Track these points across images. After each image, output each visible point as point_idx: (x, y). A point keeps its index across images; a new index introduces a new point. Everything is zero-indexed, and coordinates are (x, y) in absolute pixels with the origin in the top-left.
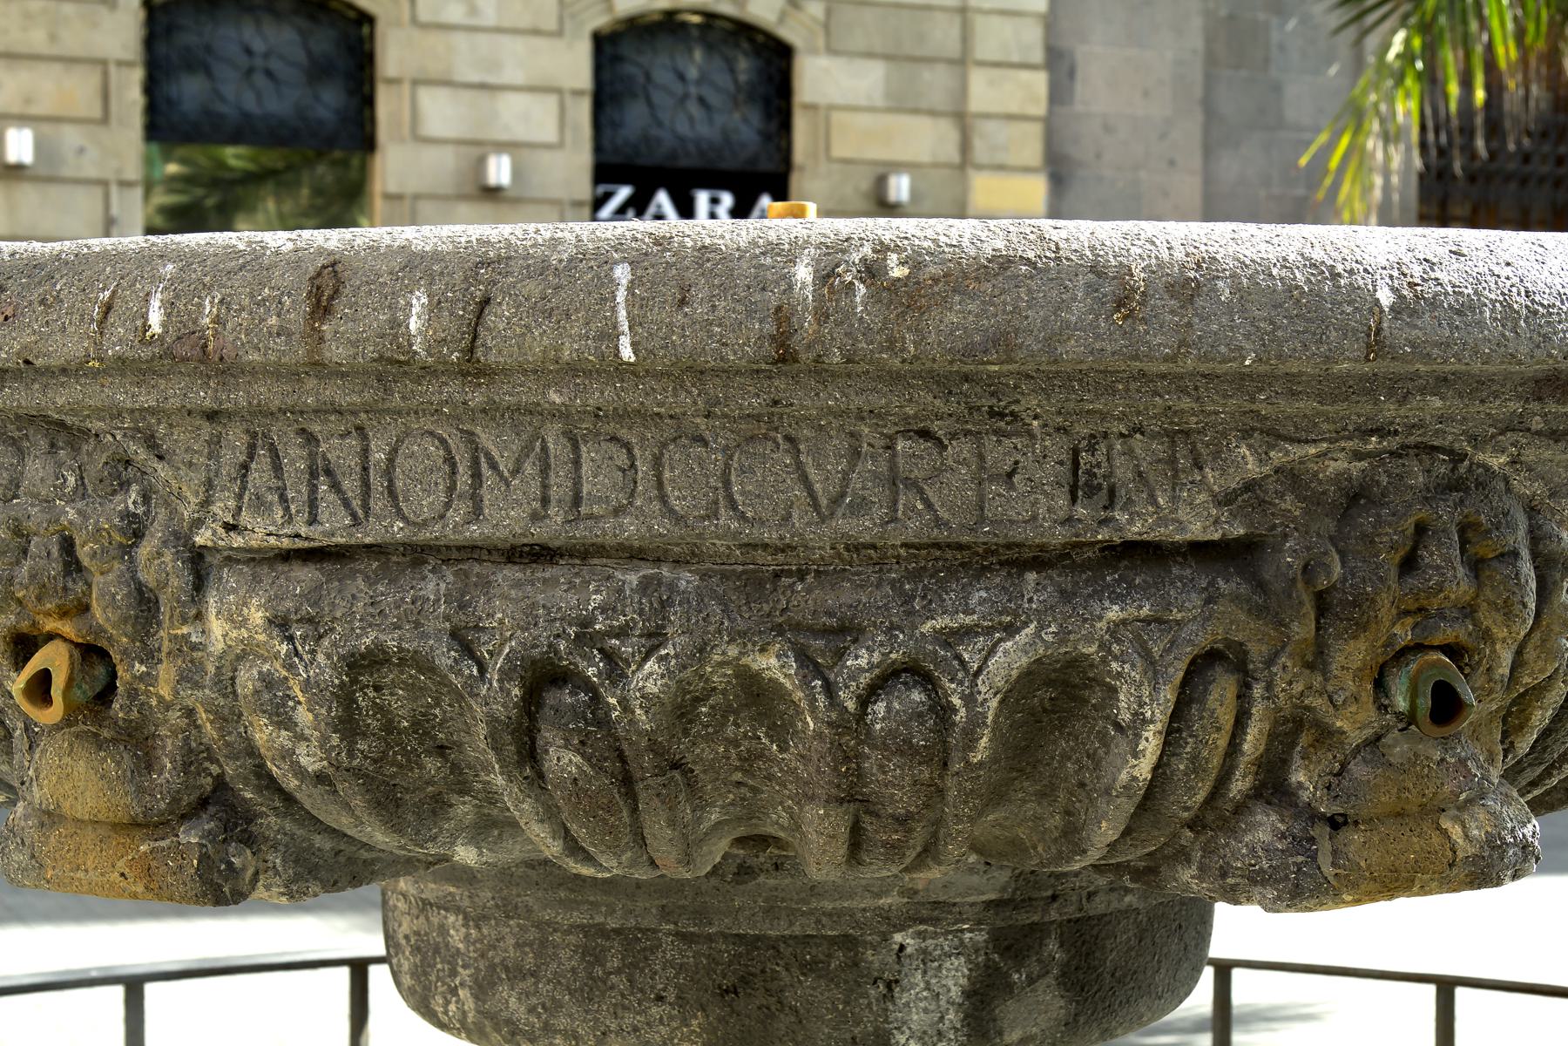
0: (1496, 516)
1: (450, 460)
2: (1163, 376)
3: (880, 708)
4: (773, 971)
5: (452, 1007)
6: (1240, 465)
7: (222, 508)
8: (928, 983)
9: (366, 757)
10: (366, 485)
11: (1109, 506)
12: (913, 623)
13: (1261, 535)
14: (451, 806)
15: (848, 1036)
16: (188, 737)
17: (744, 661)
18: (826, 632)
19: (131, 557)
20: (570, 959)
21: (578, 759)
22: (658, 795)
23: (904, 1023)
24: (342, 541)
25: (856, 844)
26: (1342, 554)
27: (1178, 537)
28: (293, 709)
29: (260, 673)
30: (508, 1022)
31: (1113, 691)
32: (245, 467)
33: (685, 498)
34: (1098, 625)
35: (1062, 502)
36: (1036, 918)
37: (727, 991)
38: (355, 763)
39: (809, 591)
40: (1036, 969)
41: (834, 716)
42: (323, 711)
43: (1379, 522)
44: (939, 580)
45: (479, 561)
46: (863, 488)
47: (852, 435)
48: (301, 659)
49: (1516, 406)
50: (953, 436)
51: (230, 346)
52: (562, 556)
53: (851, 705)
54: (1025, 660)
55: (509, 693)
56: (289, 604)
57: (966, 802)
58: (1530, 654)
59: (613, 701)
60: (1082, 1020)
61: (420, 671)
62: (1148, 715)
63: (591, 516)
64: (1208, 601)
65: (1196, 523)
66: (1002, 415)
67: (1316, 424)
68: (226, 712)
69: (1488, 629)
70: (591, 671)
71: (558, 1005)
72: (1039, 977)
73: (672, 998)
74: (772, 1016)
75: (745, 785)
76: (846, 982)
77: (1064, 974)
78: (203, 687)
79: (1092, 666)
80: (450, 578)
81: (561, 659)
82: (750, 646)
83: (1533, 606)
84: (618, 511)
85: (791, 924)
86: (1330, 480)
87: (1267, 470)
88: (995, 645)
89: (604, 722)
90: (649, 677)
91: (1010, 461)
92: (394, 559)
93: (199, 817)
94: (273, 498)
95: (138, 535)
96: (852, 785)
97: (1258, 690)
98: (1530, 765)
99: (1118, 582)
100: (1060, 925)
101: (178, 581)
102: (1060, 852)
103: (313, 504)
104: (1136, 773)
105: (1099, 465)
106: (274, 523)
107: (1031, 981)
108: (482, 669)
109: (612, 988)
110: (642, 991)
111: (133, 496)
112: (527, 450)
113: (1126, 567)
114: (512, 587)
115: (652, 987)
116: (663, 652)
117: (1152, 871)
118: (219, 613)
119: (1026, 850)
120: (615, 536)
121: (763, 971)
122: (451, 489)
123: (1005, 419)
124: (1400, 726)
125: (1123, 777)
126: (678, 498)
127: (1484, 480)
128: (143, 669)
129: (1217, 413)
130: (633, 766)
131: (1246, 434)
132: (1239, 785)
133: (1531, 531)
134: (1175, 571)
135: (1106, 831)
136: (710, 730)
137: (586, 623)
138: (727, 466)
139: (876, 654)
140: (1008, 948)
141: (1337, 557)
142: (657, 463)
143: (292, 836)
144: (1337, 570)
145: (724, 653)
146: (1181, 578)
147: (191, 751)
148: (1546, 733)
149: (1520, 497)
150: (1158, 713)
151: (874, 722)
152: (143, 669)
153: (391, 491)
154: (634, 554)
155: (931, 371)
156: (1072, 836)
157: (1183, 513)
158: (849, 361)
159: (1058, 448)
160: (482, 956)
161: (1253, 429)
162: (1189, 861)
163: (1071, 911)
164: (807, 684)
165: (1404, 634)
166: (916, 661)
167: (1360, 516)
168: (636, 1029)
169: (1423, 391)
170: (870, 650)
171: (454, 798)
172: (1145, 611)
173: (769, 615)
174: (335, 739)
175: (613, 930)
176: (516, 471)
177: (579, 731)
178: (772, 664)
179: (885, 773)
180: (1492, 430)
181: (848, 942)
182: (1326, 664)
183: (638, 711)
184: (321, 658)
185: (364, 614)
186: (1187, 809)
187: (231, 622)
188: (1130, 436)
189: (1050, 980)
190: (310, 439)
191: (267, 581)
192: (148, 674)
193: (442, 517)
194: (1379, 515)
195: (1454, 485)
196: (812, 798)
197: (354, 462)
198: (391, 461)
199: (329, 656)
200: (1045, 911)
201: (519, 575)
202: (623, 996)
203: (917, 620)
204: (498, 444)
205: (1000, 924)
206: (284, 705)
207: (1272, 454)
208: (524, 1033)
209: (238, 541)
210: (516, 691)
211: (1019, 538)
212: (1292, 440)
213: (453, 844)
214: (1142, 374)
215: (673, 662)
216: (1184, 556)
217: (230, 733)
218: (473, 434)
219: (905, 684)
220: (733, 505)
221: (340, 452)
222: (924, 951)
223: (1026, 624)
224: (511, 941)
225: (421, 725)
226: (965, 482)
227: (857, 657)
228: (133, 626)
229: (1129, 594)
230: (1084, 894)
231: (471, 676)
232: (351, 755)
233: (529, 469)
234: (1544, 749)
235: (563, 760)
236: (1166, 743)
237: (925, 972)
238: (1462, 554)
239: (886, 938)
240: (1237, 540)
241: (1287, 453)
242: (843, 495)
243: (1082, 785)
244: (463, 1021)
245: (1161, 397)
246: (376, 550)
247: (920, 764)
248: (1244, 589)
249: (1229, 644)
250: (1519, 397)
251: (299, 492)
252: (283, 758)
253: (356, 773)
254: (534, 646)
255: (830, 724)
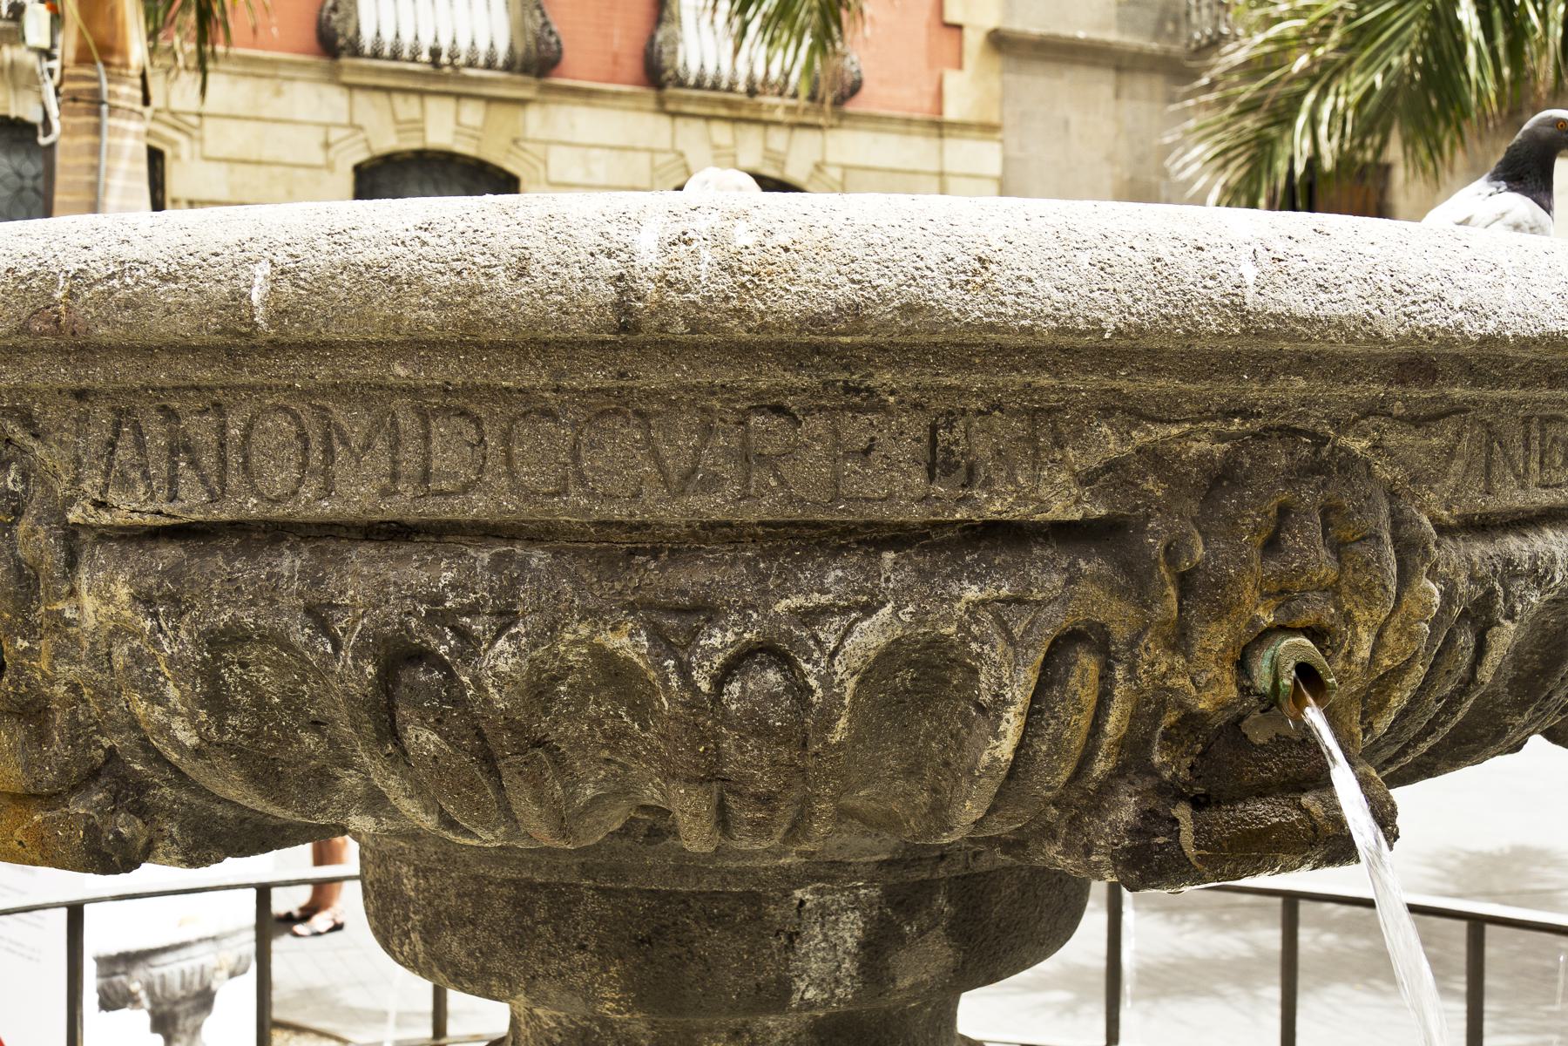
0: (1358, 500)
1: (302, 436)
2: (1021, 351)
3: (735, 688)
4: (685, 924)
5: (406, 948)
6: (1101, 442)
7: (91, 484)
8: (825, 935)
9: (238, 733)
10: (223, 461)
11: (969, 483)
12: (767, 602)
13: (1122, 516)
14: (337, 779)
15: (752, 983)
16: (75, 711)
17: (597, 640)
18: (679, 611)
19: (11, 534)
20: (503, 909)
21: (435, 737)
22: (520, 773)
23: (804, 971)
24: (200, 517)
25: (724, 820)
26: (1205, 535)
27: (1038, 517)
28: (164, 684)
29: (130, 649)
30: (452, 964)
31: (975, 672)
32: (112, 444)
33: (534, 474)
34: (957, 605)
35: (919, 479)
36: (925, 876)
37: (642, 941)
38: (226, 738)
39: (662, 569)
40: (926, 921)
41: (687, 695)
42: (188, 687)
43: (1242, 504)
44: (796, 559)
45: (337, 538)
46: (715, 464)
47: (703, 410)
48: (165, 636)
49: (1378, 390)
50: (808, 411)
51: (81, 320)
52: (418, 533)
53: (705, 686)
54: (883, 641)
55: (363, 672)
56: (152, 581)
57: (827, 783)
58: (1390, 637)
59: (465, 679)
60: (969, 966)
61: (281, 649)
62: (1009, 696)
63: (441, 493)
64: (1069, 581)
65: (1063, 504)
66: (857, 391)
67: (1178, 405)
68: (105, 687)
69: (1349, 612)
70: (443, 649)
71: (493, 951)
72: (929, 929)
73: (592, 946)
74: (684, 965)
75: (615, 762)
76: (750, 934)
77: (951, 926)
78: (80, 662)
79: (952, 646)
80: (306, 555)
81: (413, 637)
82: (601, 625)
83: (1393, 588)
84: (465, 489)
85: (699, 881)
86: (1192, 462)
87: (1128, 449)
88: (851, 625)
89: (459, 701)
90: (502, 657)
91: (865, 438)
92: (255, 535)
93: (88, 789)
94: (135, 475)
95: (18, 513)
96: (711, 765)
97: (1120, 673)
98: (1387, 744)
99: (977, 562)
100: (949, 881)
101: (53, 557)
102: (930, 828)
103: (173, 481)
104: (997, 754)
105: (957, 443)
106: (137, 500)
107: (921, 932)
108: (337, 646)
109: (540, 936)
110: (566, 940)
111: (13, 474)
112: (378, 425)
113: (986, 548)
114: (365, 564)
115: (575, 936)
116: (514, 631)
117: (1022, 844)
118: (89, 589)
119: (900, 823)
120: (464, 512)
121: (675, 924)
122: (303, 465)
123: (865, 400)
124: (1264, 706)
125: (985, 758)
126: (527, 474)
127: (1348, 462)
128: (26, 644)
129: (1078, 391)
130: (492, 744)
131: (1107, 412)
132: (1101, 766)
133: (1392, 515)
134: (1037, 551)
135: (970, 811)
136: (572, 709)
137: (437, 600)
138: (576, 441)
139: (729, 634)
140: (901, 903)
141: (1199, 538)
142: (506, 438)
143: (190, 805)
144: (1200, 552)
145: (575, 632)
146: (1042, 558)
147: (79, 724)
148: (1404, 714)
149: (1382, 482)
150: (1019, 694)
151: (729, 702)
152: (26, 644)
153: (245, 466)
154: (486, 532)
155: (781, 343)
156: (939, 813)
157: (1044, 491)
158: (693, 331)
159: (915, 426)
160: (430, 904)
161: (1114, 408)
162: (1054, 837)
163: (958, 869)
164: (660, 664)
165: (1267, 618)
166: (771, 641)
167: (1223, 497)
168: (561, 975)
169: (1287, 370)
170: (724, 630)
171: (339, 772)
172: (1005, 592)
173: (620, 593)
174: (203, 715)
175: (541, 884)
176: (367, 446)
177: (434, 709)
178: (626, 642)
179: (743, 753)
180: (1354, 414)
181: (753, 899)
182: (1189, 646)
183: (491, 690)
184: (183, 634)
185: (229, 591)
186: (1050, 789)
187: (99, 600)
188: (989, 413)
189: (939, 931)
190: (170, 414)
191: (133, 557)
192: (31, 649)
193: (295, 493)
194: (1242, 497)
195: (1315, 468)
196: (674, 776)
197: (211, 438)
198: (246, 437)
199: (190, 633)
200: (934, 870)
201: (373, 552)
202: (549, 944)
203: (771, 598)
204: (353, 421)
205: (891, 881)
206: (155, 681)
207: (1134, 433)
208: (464, 975)
209: (106, 518)
210: (370, 669)
211: (876, 517)
212: (1154, 420)
213: (345, 814)
214: (999, 348)
215: (524, 640)
216: (1046, 537)
217: (111, 708)
218: (326, 409)
219: (761, 663)
220: (581, 479)
221: (200, 429)
222: (822, 906)
223: (883, 604)
224: (453, 891)
225: (291, 700)
226: (819, 459)
227: (710, 637)
228: (14, 601)
229: (988, 574)
230: (970, 853)
231: (325, 653)
232: (221, 730)
233: (379, 445)
234: (1401, 729)
235: (423, 738)
236: (1027, 724)
237: (823, 925)
238: (1324, 537)
239: (787, 894)
240: (1100, 520)
241: (1149, 433)
242: (694, 471)
243: (947, 764)
244: (415, 961)
245: (1019, 371)
246: (238, 528)
247: (778, 744)
248: (1106, 570)
249: (1091, 625)
250: (1382, 380)
251: (159, 468)
252: (161, 732)
253: (230, 748)
254: (387, 624)
255: (684, 705)
